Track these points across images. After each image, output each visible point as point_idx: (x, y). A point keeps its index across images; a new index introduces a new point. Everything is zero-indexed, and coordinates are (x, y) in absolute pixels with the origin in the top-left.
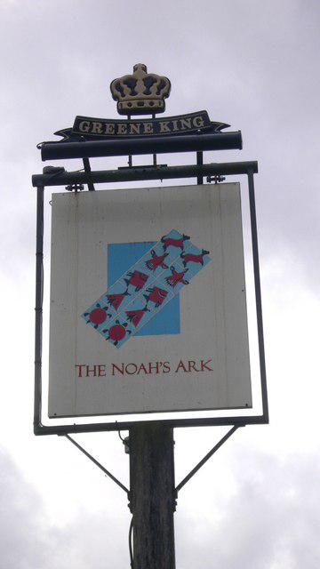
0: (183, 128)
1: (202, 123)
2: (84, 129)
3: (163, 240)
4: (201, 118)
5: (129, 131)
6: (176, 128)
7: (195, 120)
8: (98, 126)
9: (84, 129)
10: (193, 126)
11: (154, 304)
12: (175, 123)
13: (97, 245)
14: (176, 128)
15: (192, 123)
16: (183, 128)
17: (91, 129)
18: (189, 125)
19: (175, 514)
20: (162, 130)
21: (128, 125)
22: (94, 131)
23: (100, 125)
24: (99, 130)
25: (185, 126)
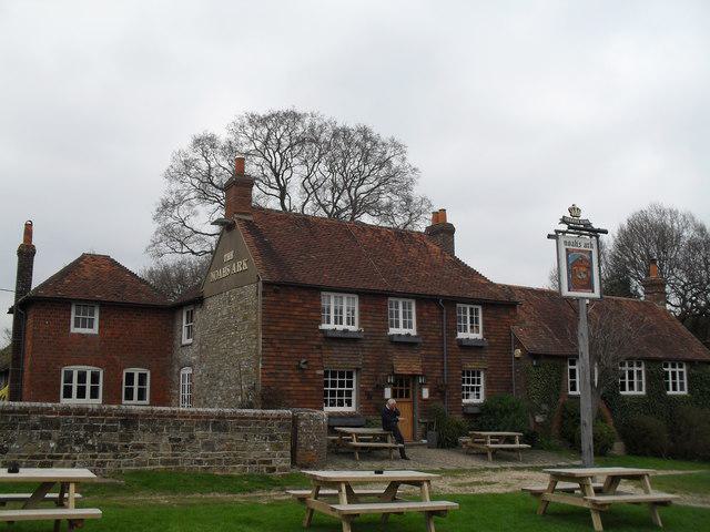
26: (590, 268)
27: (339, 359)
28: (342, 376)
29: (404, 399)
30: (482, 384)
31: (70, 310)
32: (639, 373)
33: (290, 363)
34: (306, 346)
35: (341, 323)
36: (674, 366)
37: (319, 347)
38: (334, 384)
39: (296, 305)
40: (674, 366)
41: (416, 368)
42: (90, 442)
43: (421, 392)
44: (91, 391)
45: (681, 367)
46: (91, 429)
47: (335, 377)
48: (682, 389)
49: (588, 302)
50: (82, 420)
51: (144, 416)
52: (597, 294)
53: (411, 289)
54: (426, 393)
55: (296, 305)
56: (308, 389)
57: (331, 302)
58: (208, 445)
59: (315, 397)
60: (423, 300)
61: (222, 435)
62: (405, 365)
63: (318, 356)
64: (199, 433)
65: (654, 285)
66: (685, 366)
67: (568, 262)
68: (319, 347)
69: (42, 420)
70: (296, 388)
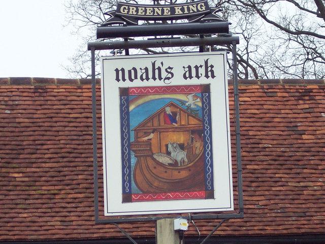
0: (191, 11)
1: (204, 8)
2: (124, 11)
3: (89, 49)
4: (203, 4)
5: (154, 13)
6: (186, 11)
7: (199, 5)
8: (133, 9)
9: (202, 9)
10: (198, 10)
11: (230, 26)
12: (186, 7)
13: (73, 59)
14: (186, 11)
15: (197, 7)
16: (191, 11)
17: (129, 12)
18: (160, 13)
19: (134, 49)
20: (177, 13)
21: (145, 8)
22: (131, 13)
23: (135, 9)
24: (135, 13)
25: (192, 10)
26: (203, 132)
49: (182, 224)
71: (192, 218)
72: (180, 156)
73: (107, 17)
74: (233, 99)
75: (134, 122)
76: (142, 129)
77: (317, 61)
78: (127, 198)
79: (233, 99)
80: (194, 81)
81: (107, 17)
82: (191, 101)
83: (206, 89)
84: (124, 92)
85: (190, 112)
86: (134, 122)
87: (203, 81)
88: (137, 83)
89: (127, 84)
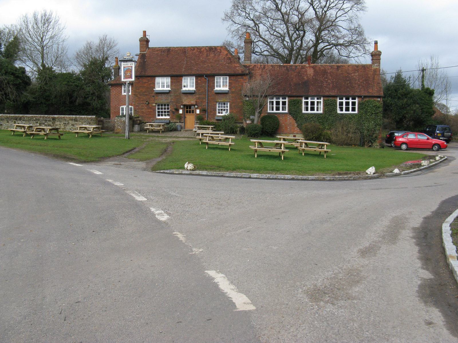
26: (131, 72)
27: (163, 99)
28: (165, 105)
29: (191, 114)
30: (229, 108)
31: (122, 87)
32: (284, 103)
33: (144, 102)
34: (149, 96)
35: (164, 87)
36: (347, 98)
37: (153, 96)
38: (165, 109)
39: (145, 83)
40: (347, 98)
41: (193, 102)
42: (46, 124)
43: (196, 111)
44: (124, 110)
45: (354, 98)
46: (46, 121)
47: (307, 99)
48: (353, 109)
49: (128, 82)
50: (44, 119)
51: (57, 118)
52: (133, 79)
53: (193, 73)
54: (198, 111)
55: (145, 83)
56: (150, 110)
57: (159, 80)
58: (73, 125)
59: (152, 113)
60: (198, 76)
61: (76, 122)
62: (187, 101)
63: (153, 99)
64: (70, 122)
65: (138, 76)
66: (287, 99)
67: (124, 70)
68: (153, 96)
69: (36, 119)
70: (146, 110)
71: (129, 81)
72: (129, 74)
73: (431, 213)
74: (181, 100)
75: (125, 70)
76: (125, 71)
77: (256, 42)
78: (124, 79)
79: (181, 100)
80: (131, 66)
81: (431, 213)
82: (130, 68)
83: (132, 66)
84: (124, 67)
85: (130, 69)
86: (125, 70)
87: (132, 65)
88: (125, 66)
89: (124, 66)
